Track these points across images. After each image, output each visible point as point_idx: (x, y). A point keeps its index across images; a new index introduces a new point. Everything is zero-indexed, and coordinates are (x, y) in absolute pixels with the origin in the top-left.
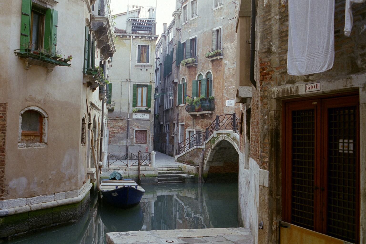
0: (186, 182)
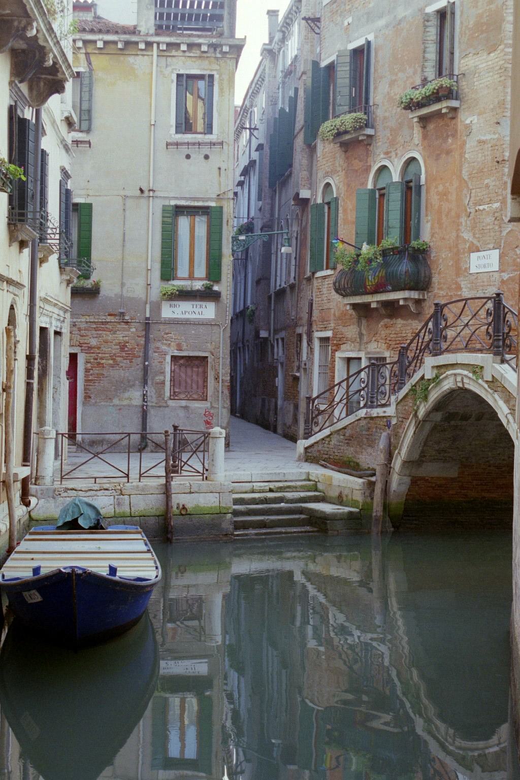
0: (330, 532)
